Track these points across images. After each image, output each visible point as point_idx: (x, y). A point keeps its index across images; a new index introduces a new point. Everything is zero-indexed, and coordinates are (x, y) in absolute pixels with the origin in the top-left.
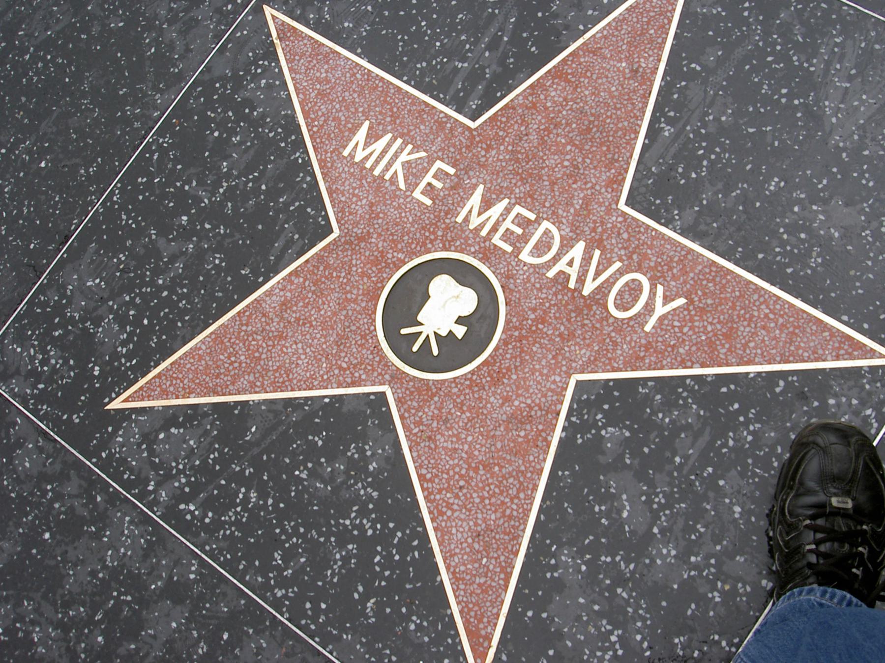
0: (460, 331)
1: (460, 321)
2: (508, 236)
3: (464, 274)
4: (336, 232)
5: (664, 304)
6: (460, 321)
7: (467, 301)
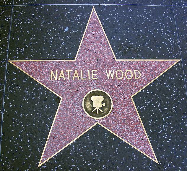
0: (104, 104)
3: (97, 93)
6: (102, 103)
7: (101, 98)
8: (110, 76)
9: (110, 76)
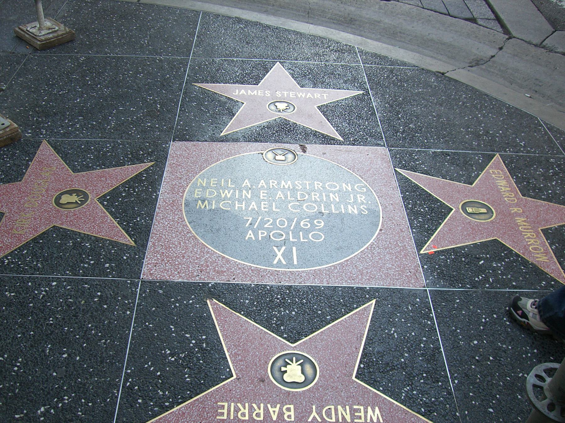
2: (359, 411)
3: (294, 384)
5: (314, 417)
6: (286, 372)
8: (374, 412)
9: (374, 412)
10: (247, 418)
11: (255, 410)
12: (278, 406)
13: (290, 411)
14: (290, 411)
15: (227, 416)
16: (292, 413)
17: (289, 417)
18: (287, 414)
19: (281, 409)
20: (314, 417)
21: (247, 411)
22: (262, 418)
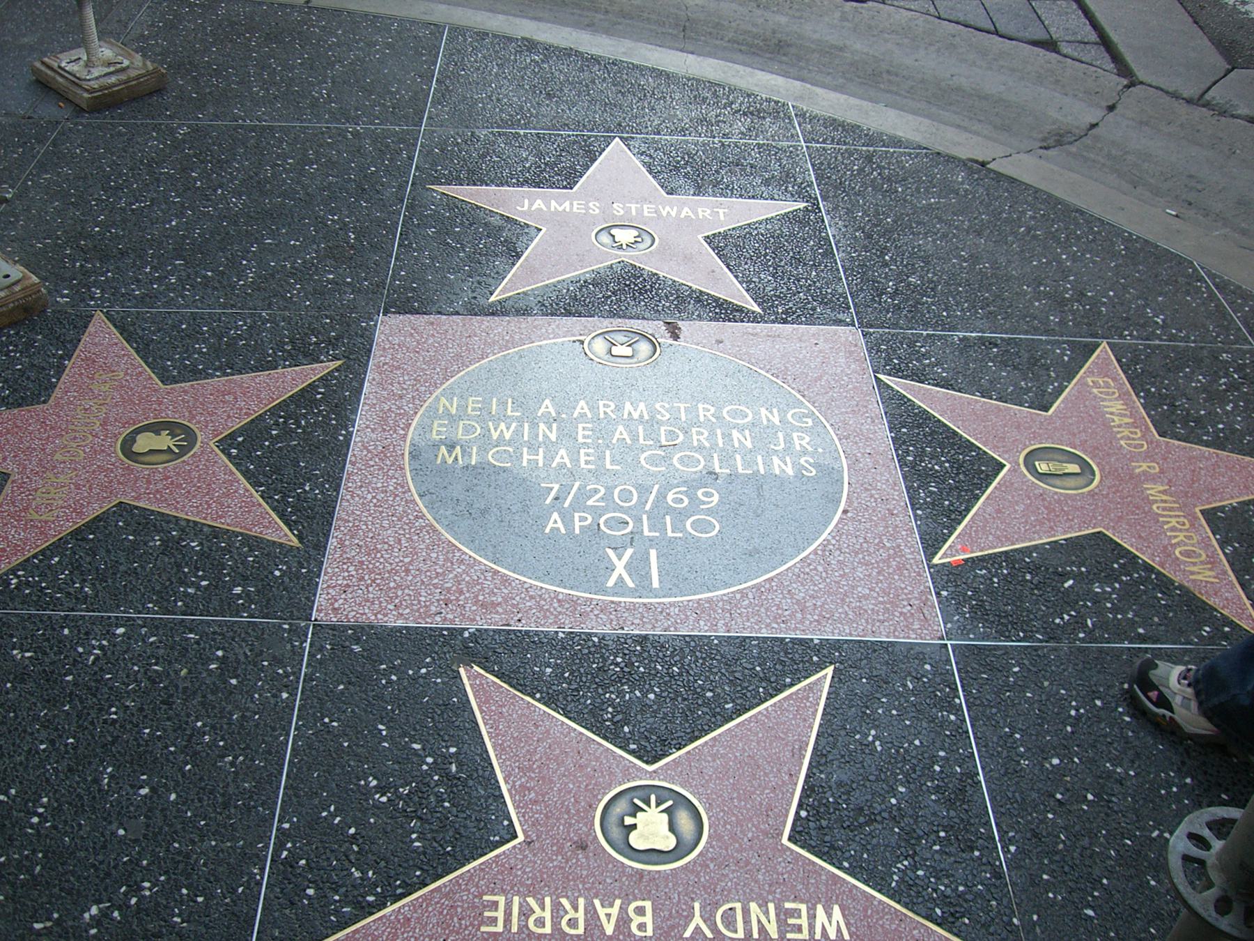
1: (634, 827)
2: (796, 913)
3: (653, 855)
4: (521, 837)
5: (698, 928)
6: (634, 827)
7: (636, 840)
8: (829, 916)
9: (829, 916)
10: (548, 930)
11: (566, 912)
12: (618, 902)
13: (644, 914)
14: (644, 914)
15: (505, 926)
16: (648, 919)
17: (642, 927)
18: (637, 920)
19: (623, 909)
20: (698, 928)
21: (547, 915)
22: (581, 931)
